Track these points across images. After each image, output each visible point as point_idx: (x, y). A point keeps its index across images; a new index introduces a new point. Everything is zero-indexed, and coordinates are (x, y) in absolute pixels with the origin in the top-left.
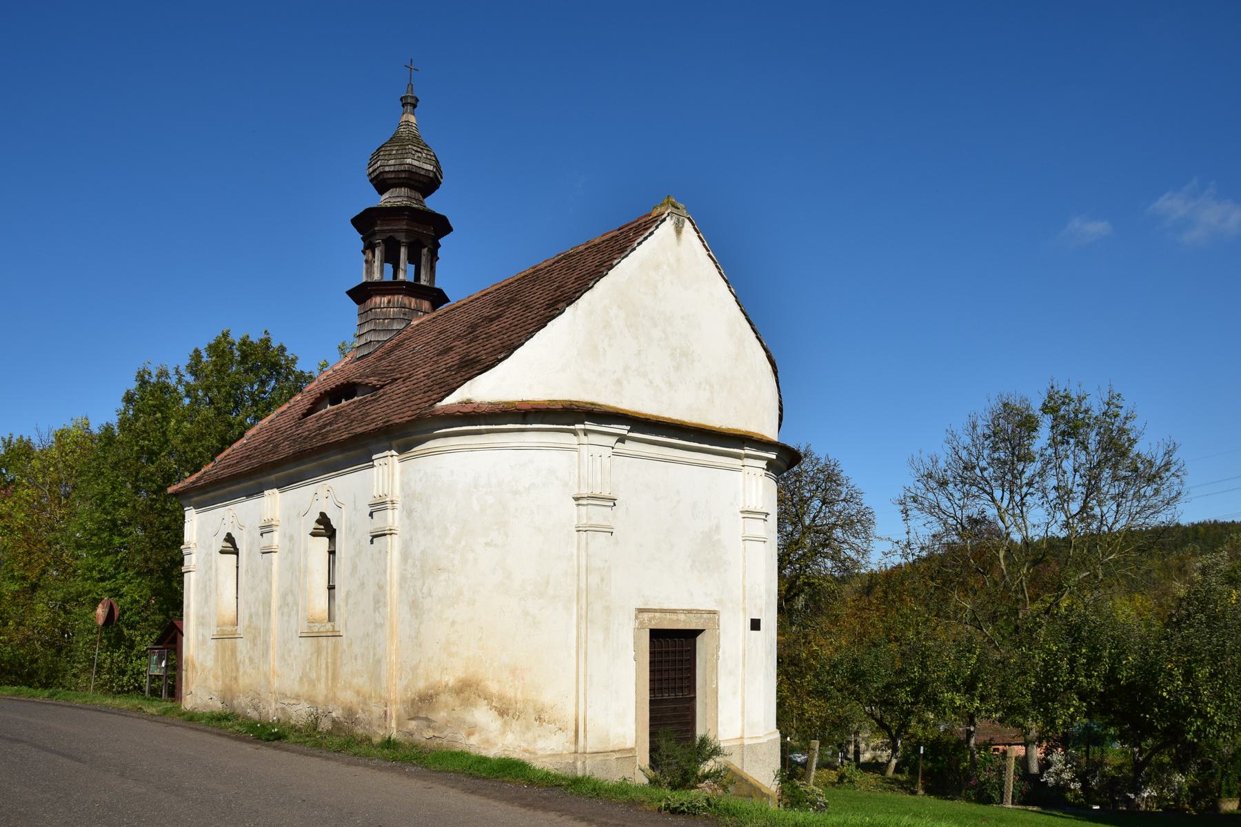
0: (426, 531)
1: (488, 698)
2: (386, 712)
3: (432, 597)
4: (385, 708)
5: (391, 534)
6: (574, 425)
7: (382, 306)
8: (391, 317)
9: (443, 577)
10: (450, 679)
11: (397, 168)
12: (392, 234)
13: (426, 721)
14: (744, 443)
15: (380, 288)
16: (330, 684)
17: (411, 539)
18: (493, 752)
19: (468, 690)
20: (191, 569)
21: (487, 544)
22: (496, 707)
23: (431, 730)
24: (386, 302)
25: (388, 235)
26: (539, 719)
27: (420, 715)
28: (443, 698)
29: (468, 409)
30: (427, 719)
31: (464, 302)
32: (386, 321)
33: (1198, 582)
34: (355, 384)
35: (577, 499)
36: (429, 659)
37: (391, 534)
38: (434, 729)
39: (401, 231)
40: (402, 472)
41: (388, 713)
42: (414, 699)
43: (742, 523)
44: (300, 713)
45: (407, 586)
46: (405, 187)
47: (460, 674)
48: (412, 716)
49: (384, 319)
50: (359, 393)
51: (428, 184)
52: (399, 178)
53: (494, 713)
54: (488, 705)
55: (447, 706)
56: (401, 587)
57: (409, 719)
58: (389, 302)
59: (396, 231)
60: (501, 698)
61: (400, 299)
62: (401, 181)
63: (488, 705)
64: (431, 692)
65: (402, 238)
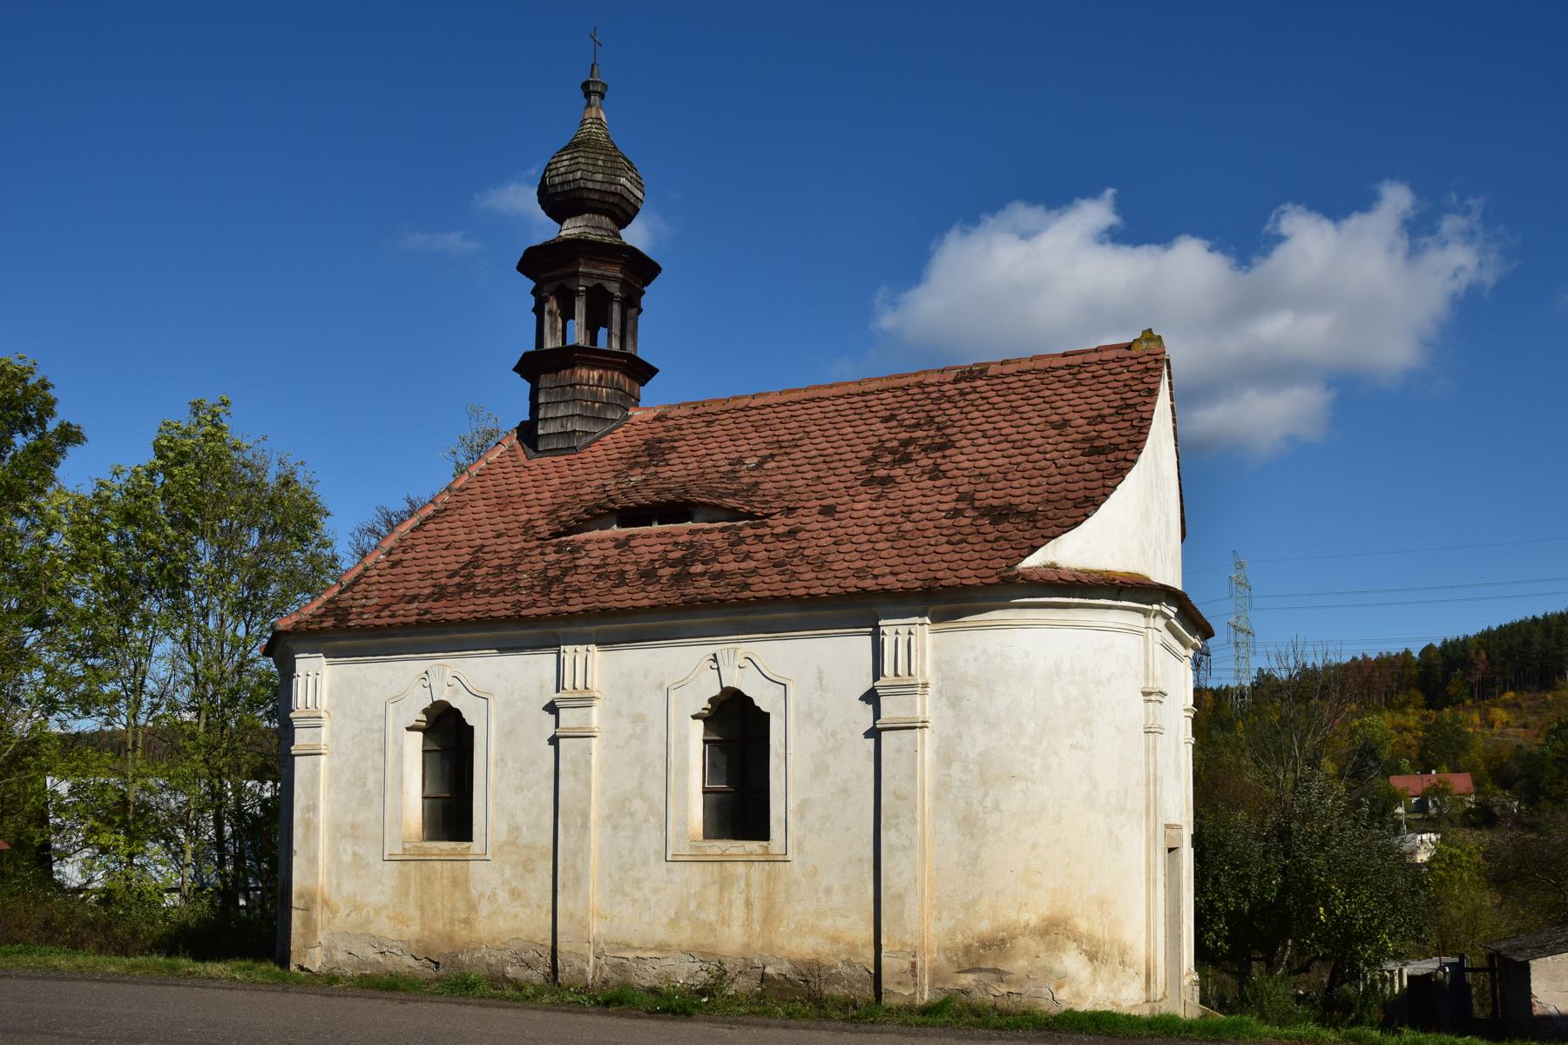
0: (987, 726)
1: (1077, 940)
2: (914, 965)
3: (1001, 811)
4: (913, 959)
5: (922, 727)
6: (1151, 604)
7: (591, 383)
8: (605, 400)
9: (1018, 786)
10: (1032, 918)
11: (606, 187)
12: (601, 281)
13: (994, 973)
14: (1197, 630)
15: (592, 357)
16: (758, 929)
17: (960, 735)
18: (1085, 1006)
19: (1054, 930)
20: (323, 751)
21: (1072, 746)
22: (1086, 951)
23: (1003, 985)
24: (596, 378)
25: (596, 282)
26: (1123, 963)
27: (983, 966)
28: (1022, 942)
29: (1053, 576)
30: (995, 971)
31: (771, 400)
32: (597, 405)
33: (206, 761)
34: (688, 503)
35: (1145, 694)
36: (997, 892)
37: (922, 727)
38: (1009, 983)
39: (615, 279)
40: (935, 647)
41: (919, 965)
42: (971, 945)
43: (927, 714)
44: (685, 972)
45: (951, 796)
46: (606, 215)
47: (1045, 911)
48: (967, 967)
49: (594, 402)
50: (696, 517)
51: (623, 213)
52: (604, 202)
53: (1084, 958)
54: (1078, 948)
55: (1027, 952)
56: (938, 797)
57: (958, 972)
58: (600, 378)
59: (608, 278)
60: (1090, 939)
61: (616, 378)
62: (606, 206)
63: (1078, 948)
64: (1001, 935)
65: (614, 288)
